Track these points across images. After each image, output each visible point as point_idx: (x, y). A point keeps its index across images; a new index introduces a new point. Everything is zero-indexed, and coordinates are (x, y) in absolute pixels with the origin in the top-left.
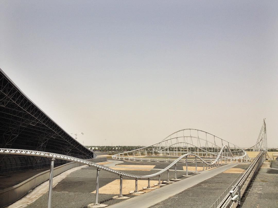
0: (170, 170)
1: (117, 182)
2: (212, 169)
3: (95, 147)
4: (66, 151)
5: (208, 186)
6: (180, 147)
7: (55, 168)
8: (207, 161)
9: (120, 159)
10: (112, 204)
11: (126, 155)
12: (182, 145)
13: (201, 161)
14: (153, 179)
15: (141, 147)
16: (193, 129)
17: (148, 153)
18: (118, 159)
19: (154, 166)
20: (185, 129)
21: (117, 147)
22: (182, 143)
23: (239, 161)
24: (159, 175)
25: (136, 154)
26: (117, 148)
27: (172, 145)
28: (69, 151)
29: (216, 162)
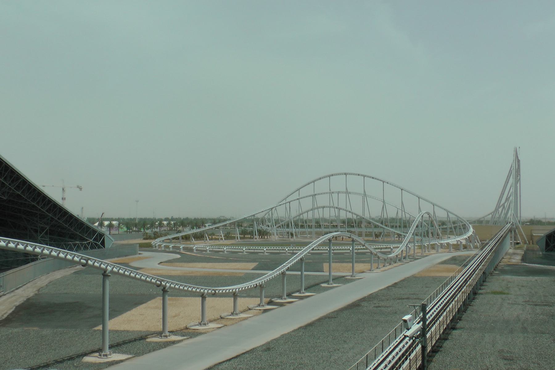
0: (288, 273)
1: (158, 301)
2: (390, 267)
3: (111, 220)
4: (36, 231)
5: (376, 307)
8: (382, 250)
9: (171, 250)
10: (143, 353)
11: (186, 238)
12: (327, 214)
13: (367, 249)
14: (247, 293)
15: (225, 220)
17: (244, 233)
18: (166, 250)
19: (254, 265)
21: (166, 219)
22: (326, 207)
23: (457, 247)
24: (261, 286)
25: (214, 237)
26: (165, 223)
27: (302, 214)
28: (43, 229)
29: (402, 251)
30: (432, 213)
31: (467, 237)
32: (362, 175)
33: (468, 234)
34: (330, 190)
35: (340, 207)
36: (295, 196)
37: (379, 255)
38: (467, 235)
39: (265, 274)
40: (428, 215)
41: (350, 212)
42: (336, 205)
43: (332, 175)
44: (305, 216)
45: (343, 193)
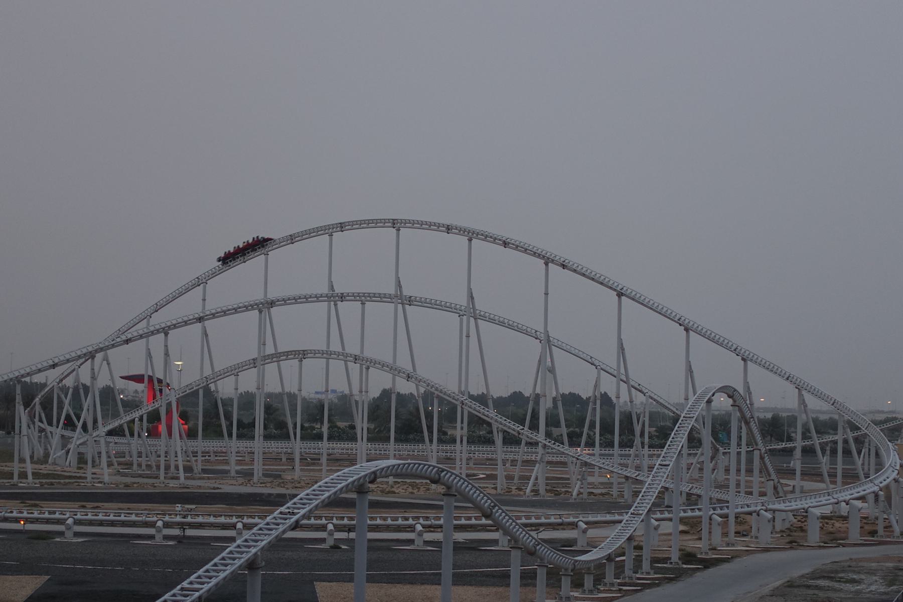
6: (292, 397)
7: (640, 490)
16: (296, 300)
20: (112, 364)
30: (741, 389)
31: (876, 489)
32: (462, 231)
33: (881, 479)
34: (332, 288)
35: (368, 354)
36: (190, 305)
37: (546, 552)
38: (876, 482)
39: (41, 446)
40: (729, 396)
41: (409, 377)
42: (353, 349)
43: (342, 227)
44: (226, 389)
45: (381, 298)
